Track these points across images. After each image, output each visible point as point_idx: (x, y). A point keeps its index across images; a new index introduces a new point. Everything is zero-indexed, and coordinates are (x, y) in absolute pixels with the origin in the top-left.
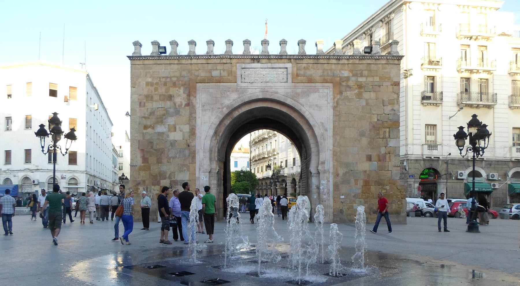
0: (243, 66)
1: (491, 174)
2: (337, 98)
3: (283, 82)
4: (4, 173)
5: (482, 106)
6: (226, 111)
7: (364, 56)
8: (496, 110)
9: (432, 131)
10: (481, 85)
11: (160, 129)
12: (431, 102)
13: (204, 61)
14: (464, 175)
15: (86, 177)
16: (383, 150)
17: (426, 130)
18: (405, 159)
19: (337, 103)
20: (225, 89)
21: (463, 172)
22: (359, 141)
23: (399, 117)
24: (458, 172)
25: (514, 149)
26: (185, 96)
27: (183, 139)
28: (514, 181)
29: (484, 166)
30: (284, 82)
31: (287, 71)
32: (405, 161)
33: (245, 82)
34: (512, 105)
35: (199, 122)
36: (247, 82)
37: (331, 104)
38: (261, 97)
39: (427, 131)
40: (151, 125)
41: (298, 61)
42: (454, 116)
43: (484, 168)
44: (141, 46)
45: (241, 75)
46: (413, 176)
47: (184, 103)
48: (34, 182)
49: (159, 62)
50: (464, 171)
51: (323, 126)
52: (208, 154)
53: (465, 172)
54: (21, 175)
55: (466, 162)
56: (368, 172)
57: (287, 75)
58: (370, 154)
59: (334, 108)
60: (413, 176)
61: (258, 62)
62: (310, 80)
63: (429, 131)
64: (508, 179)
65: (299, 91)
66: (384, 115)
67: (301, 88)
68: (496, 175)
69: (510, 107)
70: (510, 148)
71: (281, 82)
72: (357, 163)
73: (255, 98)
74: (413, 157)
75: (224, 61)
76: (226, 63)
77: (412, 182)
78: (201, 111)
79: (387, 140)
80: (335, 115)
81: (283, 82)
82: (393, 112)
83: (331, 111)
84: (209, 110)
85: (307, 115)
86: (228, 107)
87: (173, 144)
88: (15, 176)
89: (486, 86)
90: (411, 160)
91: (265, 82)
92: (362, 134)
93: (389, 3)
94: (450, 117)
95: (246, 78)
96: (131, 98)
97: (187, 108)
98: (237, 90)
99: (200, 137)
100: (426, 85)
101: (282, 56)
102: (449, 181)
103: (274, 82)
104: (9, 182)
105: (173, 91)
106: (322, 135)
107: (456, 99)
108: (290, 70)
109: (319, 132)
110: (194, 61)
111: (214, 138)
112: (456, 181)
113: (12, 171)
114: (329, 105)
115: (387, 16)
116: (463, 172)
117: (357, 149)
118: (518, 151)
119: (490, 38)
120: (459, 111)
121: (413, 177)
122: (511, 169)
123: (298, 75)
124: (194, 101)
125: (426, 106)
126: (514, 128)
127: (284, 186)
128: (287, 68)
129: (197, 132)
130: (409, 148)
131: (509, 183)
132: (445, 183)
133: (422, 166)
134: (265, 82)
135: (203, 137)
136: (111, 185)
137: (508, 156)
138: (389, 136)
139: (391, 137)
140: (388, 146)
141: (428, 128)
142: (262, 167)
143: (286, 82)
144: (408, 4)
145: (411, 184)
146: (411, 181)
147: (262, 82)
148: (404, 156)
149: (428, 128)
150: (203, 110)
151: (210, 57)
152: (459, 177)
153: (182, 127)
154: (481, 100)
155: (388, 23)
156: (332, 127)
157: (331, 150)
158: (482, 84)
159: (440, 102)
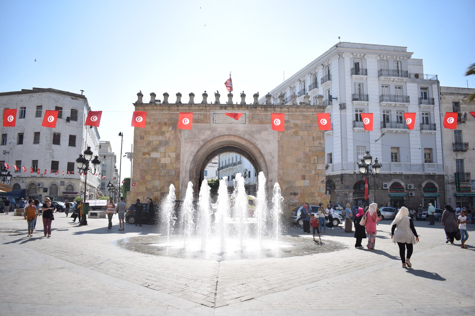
1: (409, 185)
2: (281, 135)
3: (243, 124)
4: (14, 179)
9: (362, 151)
11: (154, 155)
14: (388, 186)
20: (202, 128)
22: (296, 165)
24: (383, 184)
27: (171, 163)
30: (243, 123)
31: (246, 116)
33: (216, 123)
35: (182, 150)
36: (217, 123)
37: (277, 139)
40: (148, 152)
42: (378, 139)
44: (142, 96)
45: (213, 118)
50: (388, 183)
51: (271, 155)
52: (188, 174)
53: (388, 184)
54: (28, 181)
56: (303, 188)
57: (246, 118)
58: (304, 174)
59: (279, 142)
61: (225, 109)
65: (254, 129)
66: (314, 147)
68: (413, 186)
71: (241, 124)
72: (295, 181)
76: (203, 110)
77: (347, 192)
78: (184, 143)
79: (316, 165)
80: (279, 147)
81: (243, 124)
82: (320, 145)
84: (190, 142)
86: (203, 140)
88: (23, 182)
91: (230, 123)
92: (299, 161)
94: (376, 141)
95: (217, 121)
96: (134, 133)
98: (210, 129)
99: (183, 162)
102: (377, 191)
103: (236, 124)
104: (18, 187)
105: (164, 129)
106: (271, 161)
109: (268, 159)
113: (21, 178)
114: (275, 139)
116: (387, 184)
117: (295, 171)
121: (348, 188)
124: (179, 136)
132: (374, 193)
133: (355, 179)
134: (230, 123)
135: (185, 161)
139: (319, 162)
140: (317, 169)
143: (244, 124)
145: (347, 194)
147: (227, 123)
150: (185, 142)
151: (192, 105)
152: (384, 188)
153: (170, 154)
156: (277, 155)
157: (276, 172)
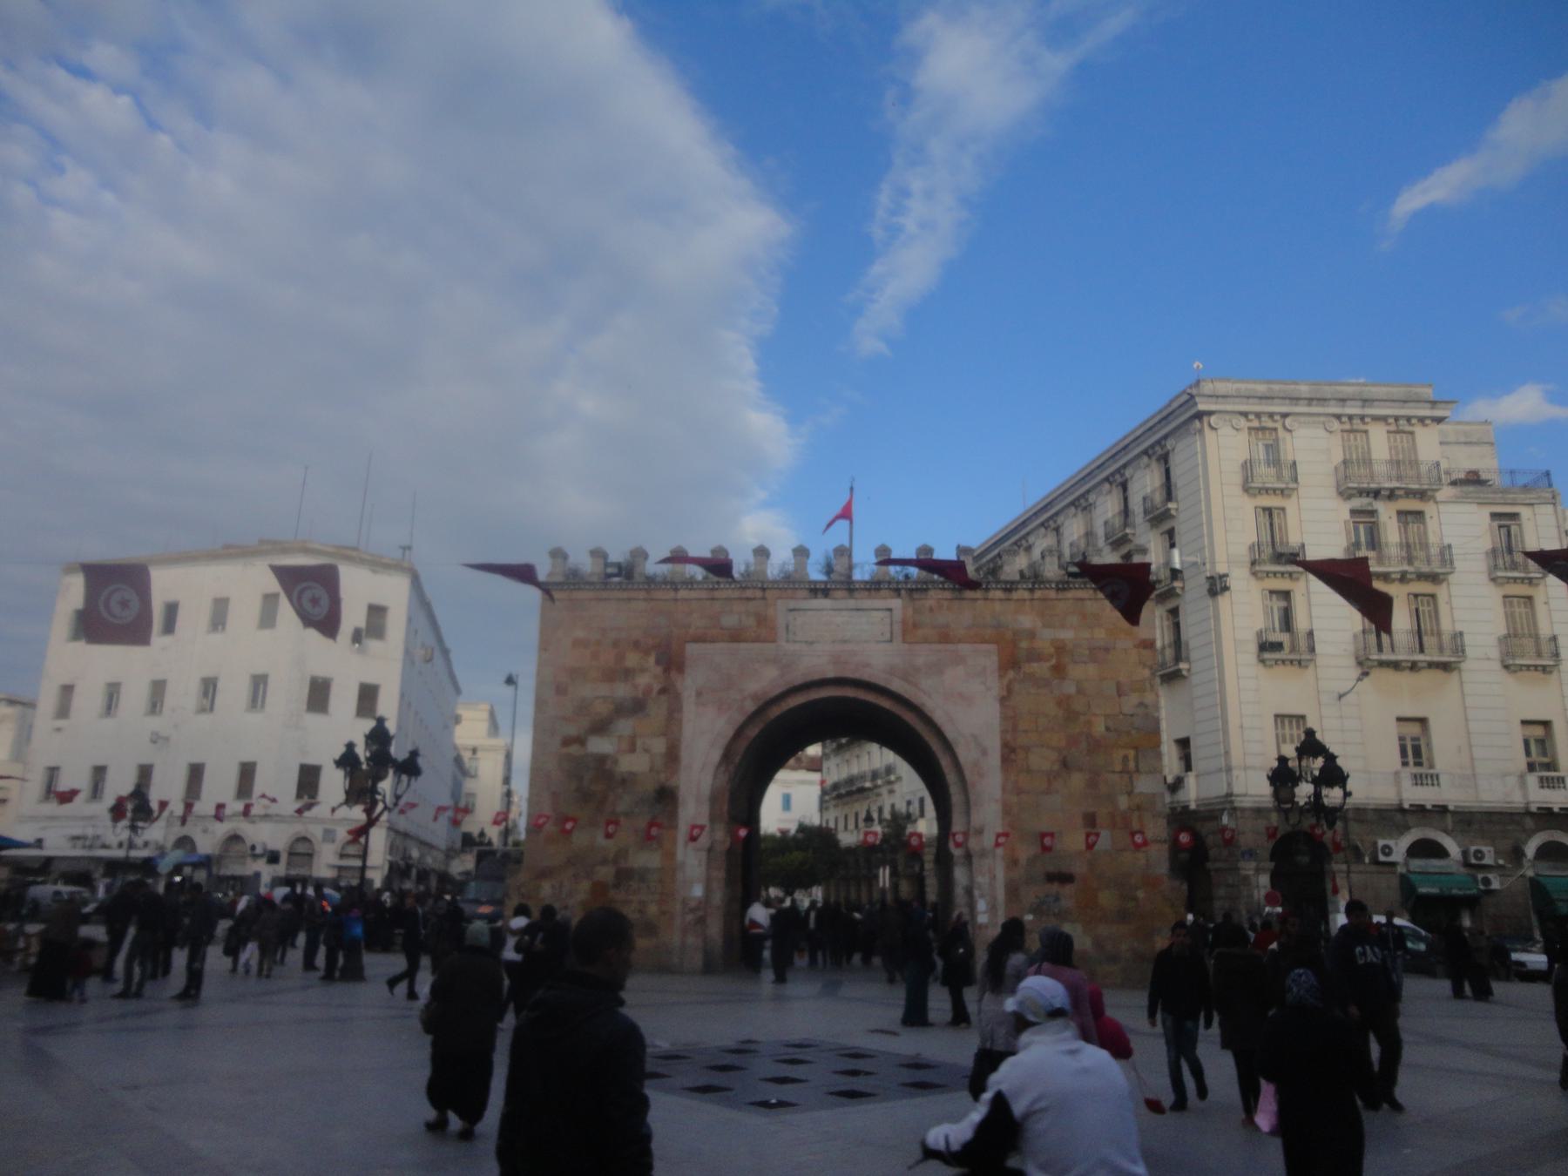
0: (792, 604)
1: (1473, 848)
5: (1425, 665)
6: (751, 707)
7: (1067, 582)
8: (1466, 676)
10: (1417, 610)
12: (1284, 657)
13: (704, 594)
15: (388, 836)
16: (1123, 802)
17: (1277, 728)
18: (1228, 806)
19: (1009, 690)
21: (1391, 843)
23: (1157, 721)
24: (1375, 844)
25: (1532, 780)
26: (659, 670)
28: (1546, 870)
29: (1450, 827)
31: (891, 617)
32: (1226, 813)
34: (1511, 662)
38: (831, 674)
39: (1280, 731)
41: (916, 595)
43: (1452, 831)
46: (1250, 854)
47: (656, 687)
48: (253, 848)
49: (605, 595)
53: (1396, 844)
55: (1399, 816)
59: (1003, 700)
60: (1250, 854)
62: (945, 637)
63: (1287, 731)
64: (1526, 864)
66: (1121, 717)
67: (924, 654)
69: (1506, 667)
70: (1522, 777)
73: (817, 677)
74: (1247, 803)
75: (749, 593)
79: (1131, 778)
80: (1004, 718)
83: (997, 706)
85: (939, 717)
86: (755, 697)
87: (627, 781)
89: (1433, 612)
90: (1243, 810)
93: (1161, 411)
94: (1341, 697)
97: (663, 698)
100: (1268, 612)
101: (879, 583)
102: (1354, 867)
107: (1351, 648)
108: (898, 615)
110: (683, 594)
111: (723, 769)
112: (1374, 868)
115: (1158, 442)
116: (1391, 843)
118: (1551, 785)
119: (1429, 493)
120: (1359, 679)
122: (1530, 834)
123: (916, 626)
125: (1271, 666)
126: (1525, 723)
127: (917, 869)
128: (890, 610)
129: (684, 755)
130: (1234, 779)
131: (1530, 873)
136: (441, 856)
137: (1516, 800)
138: (1137, 766)
141: (1283, 723)
142: (857, 815)
144: (1205, 419)
146: (1248, 867)
148: (1222, 800)
149: (1283, 723)
152: (1382, 858)
154: (1422, 650)
155: (1165, 459)
158: (1421, 609)
159: (1309, 657)
